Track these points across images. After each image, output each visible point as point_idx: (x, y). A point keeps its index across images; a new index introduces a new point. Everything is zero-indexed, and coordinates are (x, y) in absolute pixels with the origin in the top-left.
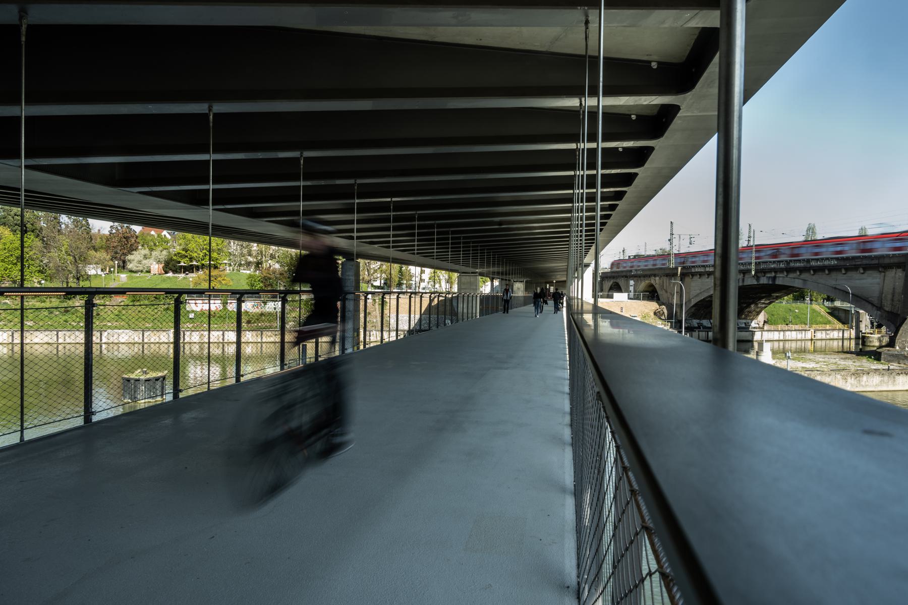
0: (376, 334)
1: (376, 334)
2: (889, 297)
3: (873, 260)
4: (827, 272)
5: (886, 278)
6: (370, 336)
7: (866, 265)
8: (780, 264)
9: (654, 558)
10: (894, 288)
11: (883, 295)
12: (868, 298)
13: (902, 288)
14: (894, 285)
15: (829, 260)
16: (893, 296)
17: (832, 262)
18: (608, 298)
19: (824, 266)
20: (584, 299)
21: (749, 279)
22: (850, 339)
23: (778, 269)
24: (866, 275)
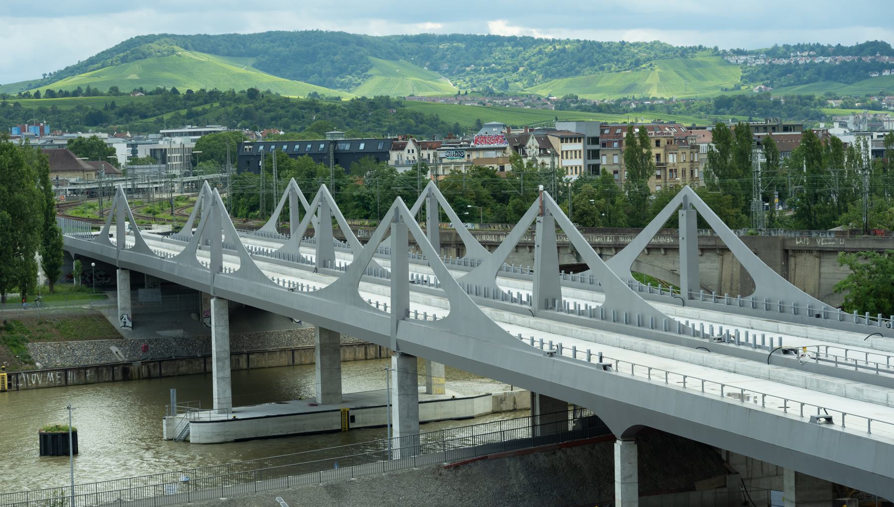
0: (26, 378)
1: (26, 378)
2: (728, 284)
3: (709, 240)
4: (663, 252)
5: (724, 262)
6: (17, 382)
7: (703, 246)
8: (606, 239)
9: (410, 297)
10: (732, 275)
11: (723, 282)
12: (707, 286)
13: (739, 275)
14: (732, 271)
15: (664, 237)
16: (732, 284)
17: (668, 239)
18: (750, 410)
19: (659, 245)
20: (753, 500)
21: (566, 256)
22: (126, 185)
23: (604, 245)
24: (704, 257)
